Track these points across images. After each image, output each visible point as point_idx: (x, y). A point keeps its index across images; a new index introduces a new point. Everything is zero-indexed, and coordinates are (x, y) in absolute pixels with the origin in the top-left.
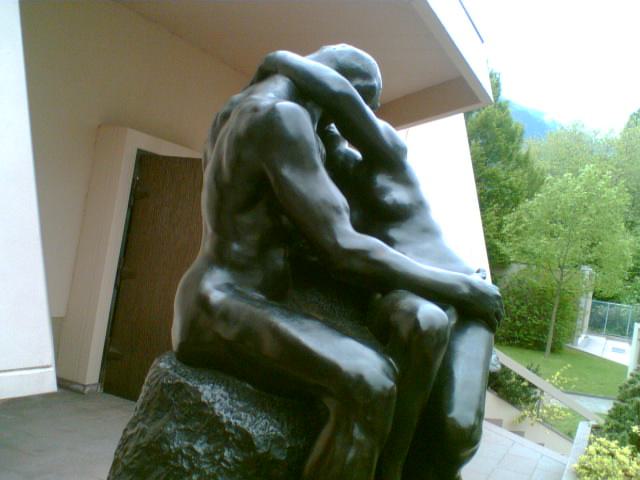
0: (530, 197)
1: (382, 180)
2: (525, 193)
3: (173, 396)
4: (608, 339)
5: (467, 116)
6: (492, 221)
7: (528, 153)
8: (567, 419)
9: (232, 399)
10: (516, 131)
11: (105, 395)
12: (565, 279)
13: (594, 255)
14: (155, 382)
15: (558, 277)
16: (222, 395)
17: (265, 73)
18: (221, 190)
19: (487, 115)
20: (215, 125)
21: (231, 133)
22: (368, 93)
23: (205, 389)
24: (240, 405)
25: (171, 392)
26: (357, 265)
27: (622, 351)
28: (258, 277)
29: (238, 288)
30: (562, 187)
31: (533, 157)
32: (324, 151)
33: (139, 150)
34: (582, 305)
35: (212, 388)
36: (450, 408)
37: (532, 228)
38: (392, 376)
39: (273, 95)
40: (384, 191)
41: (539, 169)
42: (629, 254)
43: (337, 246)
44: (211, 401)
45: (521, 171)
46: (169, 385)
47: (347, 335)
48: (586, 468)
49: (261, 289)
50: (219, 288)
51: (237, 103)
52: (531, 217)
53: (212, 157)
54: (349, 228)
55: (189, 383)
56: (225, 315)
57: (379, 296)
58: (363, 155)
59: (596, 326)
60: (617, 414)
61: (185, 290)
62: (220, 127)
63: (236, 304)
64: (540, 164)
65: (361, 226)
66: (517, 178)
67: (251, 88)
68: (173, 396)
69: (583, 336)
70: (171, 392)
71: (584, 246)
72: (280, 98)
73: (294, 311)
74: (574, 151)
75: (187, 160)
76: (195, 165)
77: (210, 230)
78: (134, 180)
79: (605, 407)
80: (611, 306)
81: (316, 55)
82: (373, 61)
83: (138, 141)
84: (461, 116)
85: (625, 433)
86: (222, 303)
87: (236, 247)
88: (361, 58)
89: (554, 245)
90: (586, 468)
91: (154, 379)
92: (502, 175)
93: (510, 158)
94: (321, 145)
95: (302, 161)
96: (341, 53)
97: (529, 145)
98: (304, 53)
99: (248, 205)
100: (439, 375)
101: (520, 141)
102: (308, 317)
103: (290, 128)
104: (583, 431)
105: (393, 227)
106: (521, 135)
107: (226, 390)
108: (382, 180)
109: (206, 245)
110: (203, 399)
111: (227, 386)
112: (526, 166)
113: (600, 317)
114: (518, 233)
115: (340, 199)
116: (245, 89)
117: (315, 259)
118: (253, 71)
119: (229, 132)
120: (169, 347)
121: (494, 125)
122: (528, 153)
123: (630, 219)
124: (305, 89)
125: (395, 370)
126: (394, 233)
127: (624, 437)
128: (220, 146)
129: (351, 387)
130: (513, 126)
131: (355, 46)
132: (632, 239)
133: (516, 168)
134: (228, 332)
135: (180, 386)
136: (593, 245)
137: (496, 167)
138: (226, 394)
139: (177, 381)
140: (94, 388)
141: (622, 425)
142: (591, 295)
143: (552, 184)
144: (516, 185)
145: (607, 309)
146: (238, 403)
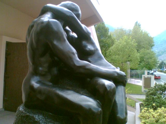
0: (112, 46)
1: (84, 43)
2: (111, 45)
3: (26, 119)
4: (135, 79)
5: (95, 26)
6: (103, 53)
7: (110, 35)
8: (130, 101)
9: (46, 119)
10: (107, 29)
11: (5, 111)
12: (123, 66)
13: (130, 59)
14: (19, 115)
15: (122, 66)
16: (42, 118)
17: (45, 11)
18: (34, 50)
19: (99, 25)
20: (29, 29)
21: (35, 31)
22: (78, 15)
23: (36, 116)
24: (49, 120)
25: (25, 118)
26: (82, 71)
27: (139, 82)
28: (49, 78)
29: (43, 82)
30: (119, 43)
31: (112, 35)
32: (67, 35)
33: (7, 42)
34: (128, 72)
35: (38, 116)
36: (117, 113)
37: (113, 54)
38: (100, 107)
39: (47, 18)
40: (86, 46)
41: (114, 38)
42: (139, 58)
43: (75, 65)
44: (39, 120)
45: (109, 39)
46: (24, 116)
47: (82, 94)
48: (142, 116)
49: (51, 81)
50: (37, 83)
51: (36, 22)
52: (113, 50)
53: (29, 40)
54: (78, 59)
55: (30, 115)
56: (39, 91)
57: (88, 79)
58: (77, 36)
59: (132, 76)
60: (147, 100)
61: (25, 84)
62: (31, 29)
63: (44, 87)
64: (114, 37)
65: (81, 58)
66: (109, 41)
67: (40, 17)
68: (26, 119)
69: (129, 79)
70: (25, 118)
71: (127, 57)
72: (49, 18)
73: (64, 88)
74: (121, 33)
75: (21, 43)
76: (24, 45)
77: (31, 64)
78: (6, 50)
79: (144, 97)
80: (135, 71)
81: (60, 4)
82: (78, 6)
83: (7, 39)
84: (94, 26)
85: (150, 106)
86: (38, 88)
87: (40, 68)
88: (74, 5)
89: (120, 57)
90: (142, 116)
91: (18, 114)
92: (105, 41)
93: (106, 36)
94: (66, 33)
95: (60, 38)
96: (68, 4)
97: (111, 32)
98: (57, 4)
99: (43, 55)
100: (114, 103)
101: (108, 32)
102: (68, 89)
103: (55, 28)
104: (138, 105)
105: (90, 57)
106: (108, 30)
107: (43, 116)
108: (84, 43)
109: (30, 69)
110: (36, 120)
111: (43, 114)
112: (110, 38)
113: (132, 74)
114: (110, 55)
115: (74, 50)
116: (38, 17)
117: (66, 69)
118: (39, 12)
119: (34, 31)
120: (22, 103)
121: (101, 28)
122: (110, 35)
123: (137, 49)
124: (57, 14)
125: (100, 104)
126: (89, 59)
127: (150, 107)
128: (32, 36)
129: (87, 112)
130: (106, 27)
131: (72, 2)
132: (139, 54)
133: (108, 39)
134: (42, 98)
135: (27, 116)
136: (129, 56)
137: (102, 39)
138: (43, 117)
139: (26, 114)
140: (2, 110)
141: (149, 104)
142: (130, 69)
143: (117, 42)
144: (108, 43)
145: (134, 72)
146: (48, 120)
